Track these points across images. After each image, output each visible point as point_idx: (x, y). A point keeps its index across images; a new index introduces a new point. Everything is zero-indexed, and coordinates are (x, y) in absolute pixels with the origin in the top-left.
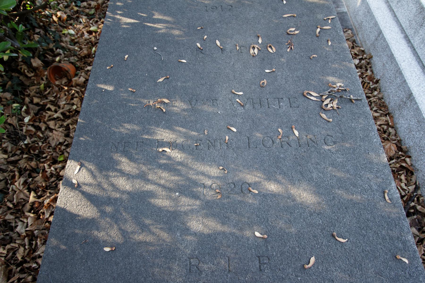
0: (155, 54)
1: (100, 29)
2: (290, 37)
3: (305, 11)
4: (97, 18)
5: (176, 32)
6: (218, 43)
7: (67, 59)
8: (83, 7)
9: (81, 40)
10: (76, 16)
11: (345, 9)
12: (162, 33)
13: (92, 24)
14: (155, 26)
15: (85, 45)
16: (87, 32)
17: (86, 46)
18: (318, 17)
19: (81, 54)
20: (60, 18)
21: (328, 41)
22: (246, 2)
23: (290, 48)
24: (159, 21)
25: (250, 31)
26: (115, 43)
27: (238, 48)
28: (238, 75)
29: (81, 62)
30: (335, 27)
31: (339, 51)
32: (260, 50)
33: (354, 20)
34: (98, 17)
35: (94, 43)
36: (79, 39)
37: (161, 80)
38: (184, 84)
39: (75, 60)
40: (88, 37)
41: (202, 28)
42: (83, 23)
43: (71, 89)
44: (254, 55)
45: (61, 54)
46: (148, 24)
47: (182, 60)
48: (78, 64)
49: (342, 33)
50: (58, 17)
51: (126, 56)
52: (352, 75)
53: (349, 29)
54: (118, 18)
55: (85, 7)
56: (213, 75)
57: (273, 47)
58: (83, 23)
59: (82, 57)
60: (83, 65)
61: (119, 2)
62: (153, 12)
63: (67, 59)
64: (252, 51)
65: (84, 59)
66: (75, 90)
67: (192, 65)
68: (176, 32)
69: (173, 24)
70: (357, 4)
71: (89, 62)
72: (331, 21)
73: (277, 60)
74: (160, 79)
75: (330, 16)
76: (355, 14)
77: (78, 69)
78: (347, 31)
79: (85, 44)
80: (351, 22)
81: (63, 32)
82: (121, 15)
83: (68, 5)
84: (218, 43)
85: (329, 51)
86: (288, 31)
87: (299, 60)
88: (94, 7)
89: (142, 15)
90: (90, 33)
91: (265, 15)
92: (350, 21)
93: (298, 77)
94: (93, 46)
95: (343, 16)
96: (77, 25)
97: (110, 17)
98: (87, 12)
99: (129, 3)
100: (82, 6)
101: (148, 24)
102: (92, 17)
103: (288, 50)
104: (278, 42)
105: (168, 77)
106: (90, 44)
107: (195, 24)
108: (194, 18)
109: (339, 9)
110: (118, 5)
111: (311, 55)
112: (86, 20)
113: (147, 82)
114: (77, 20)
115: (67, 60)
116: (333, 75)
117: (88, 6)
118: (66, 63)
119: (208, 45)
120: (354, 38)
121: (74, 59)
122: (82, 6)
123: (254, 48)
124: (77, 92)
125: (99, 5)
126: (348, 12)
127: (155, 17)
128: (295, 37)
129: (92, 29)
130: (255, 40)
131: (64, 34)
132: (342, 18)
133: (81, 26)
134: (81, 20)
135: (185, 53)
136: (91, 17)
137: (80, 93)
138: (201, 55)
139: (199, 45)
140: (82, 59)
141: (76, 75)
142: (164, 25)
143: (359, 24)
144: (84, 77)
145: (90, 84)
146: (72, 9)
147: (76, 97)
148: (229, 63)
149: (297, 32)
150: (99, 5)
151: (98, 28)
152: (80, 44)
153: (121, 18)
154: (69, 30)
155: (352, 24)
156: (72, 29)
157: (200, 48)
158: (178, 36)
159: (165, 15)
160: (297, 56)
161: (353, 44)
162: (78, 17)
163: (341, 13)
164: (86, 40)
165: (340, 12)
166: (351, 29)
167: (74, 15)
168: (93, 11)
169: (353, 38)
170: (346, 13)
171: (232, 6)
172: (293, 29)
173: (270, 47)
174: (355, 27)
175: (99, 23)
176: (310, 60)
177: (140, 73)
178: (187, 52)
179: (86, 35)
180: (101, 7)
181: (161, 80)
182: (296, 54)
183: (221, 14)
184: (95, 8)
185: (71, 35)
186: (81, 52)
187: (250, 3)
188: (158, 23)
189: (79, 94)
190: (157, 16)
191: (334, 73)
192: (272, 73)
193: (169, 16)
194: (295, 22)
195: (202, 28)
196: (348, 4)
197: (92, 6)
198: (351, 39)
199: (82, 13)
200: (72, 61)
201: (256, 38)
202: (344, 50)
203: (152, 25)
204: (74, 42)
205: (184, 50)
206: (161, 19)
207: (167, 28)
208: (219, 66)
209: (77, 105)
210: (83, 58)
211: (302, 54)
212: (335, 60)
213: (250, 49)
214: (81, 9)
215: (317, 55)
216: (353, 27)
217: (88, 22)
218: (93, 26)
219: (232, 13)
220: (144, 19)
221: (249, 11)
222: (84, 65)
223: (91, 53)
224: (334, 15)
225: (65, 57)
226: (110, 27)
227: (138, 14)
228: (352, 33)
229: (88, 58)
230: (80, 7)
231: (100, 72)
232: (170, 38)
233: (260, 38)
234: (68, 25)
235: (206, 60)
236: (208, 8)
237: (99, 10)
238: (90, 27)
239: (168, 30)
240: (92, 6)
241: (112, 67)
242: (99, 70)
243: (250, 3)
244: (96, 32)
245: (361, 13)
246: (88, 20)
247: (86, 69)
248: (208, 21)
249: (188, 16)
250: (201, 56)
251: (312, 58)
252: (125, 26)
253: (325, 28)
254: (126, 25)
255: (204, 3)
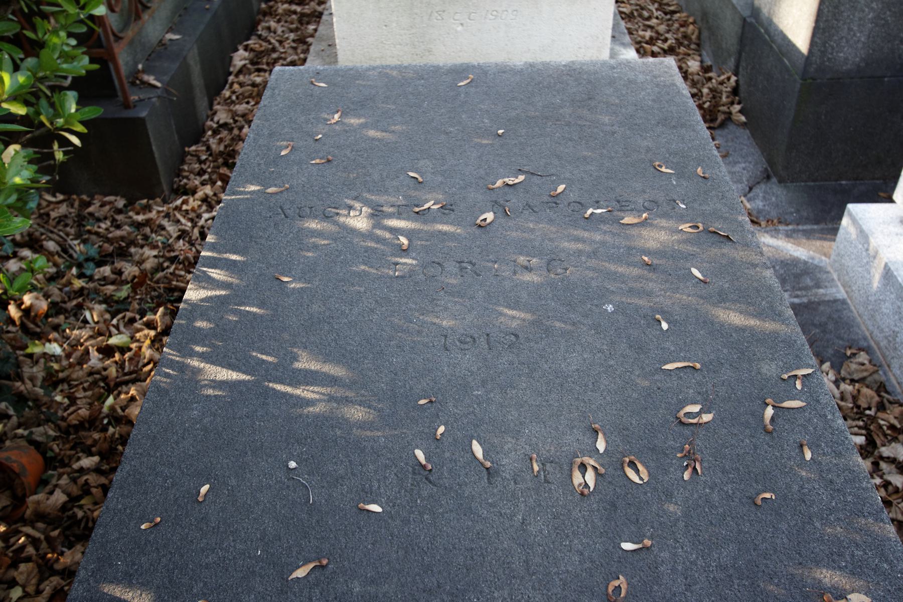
0: (291, 483)
1: (138, 341)
2: (687, 432)
3: (725, 351)
4: (132, 311)
5: (357, 413)
6: (478, 450)
7: (26, 433)
8: (99, 280)
9: (78, 373)
10: (74, 302)
11: (838, 292)
12: (317, 416)
13: (117, 327)
14: (298, 392)
15: (85, 390)
16: (99, 350)
17: (89, 393)
18: (764, 371)
19: (71, 418)
20: (27, 312)
21: (801, 446)
22: (558, 324)
23: (690, 469)
24: (309, 378)
25: (570, 412)
26: (177, 443)
27: (536, 468)
28: (537, 560)
29: (66, 441)
30: (818, 401)
31: (839, 481)
32: (601, 475)
33: (869, 323)
34: (137, 306)
35: (112, 384)
36: (71, 370)
37: (301, 573)
38: (371, 589)
39: (48, 436)
40: (100, 365)
41: (431, 402)
42: (93, 325)
43: (17, 533)
44: (586, 491)
45: (9, 417)
46: (279, 387)
47: (369, 503)
48: (55, 447)
49: (841, 421)
50: (23, 307)
51: (204, 489)
52: (890, 563)
53: (861, 349)
54: (194, 367)
55: (104, 278)
56: (461, 559)
57: (640, 467)
58: (93, 325)
59: (69, 426)
60: (68, 453)
61: (203, 320)
62: (295, 350)
63: (26, 433)
64: (577, 478)
65: (76, 432)
66: (28, 536)
67: (398, 522)
68: (357, 413)
69: (350, 388)
70: (870, 283)
71: (89, 442)
72: (803, 385)
73: (654, 508)
74: (298, 567)
75: (798, 368)
76: (870, 307)
77: (51, 462)
78: (854, 355)
79: (86, 385)
80: (864, 328)
81: (29, 351)
82: (203, 357)
83: (57, 273)
84: (478, 450)
85: (809, 480)
86: (682, 413)
87: (721, 510)
88: (129, 279)
89: (264, 357)
90: (107, 351)
91: (612, 362)
92: (859, 327)
93: (722, 568)
94: (109, 391)
95: (837, 311)
96: (72, 329)
97: (171, 364)
98: (108, 292)
99: (230, 321)
100: (96, 277)
101: (279, 387)
102: (121, 307)
103: (686, 476)
104: (653, 449)
105: (325, 562)
106: (102, 384)
107: (411, 388)
108: (411, 369)
109: (821, 291)
110: (200, 329)
111: (758, 494)
112: (101, 315)
113: (258, 579)
114: (75, 315)
115: (22, 436)
116: (832, 562)
117: (113, 276)
118: (19, 448)
119: (447, 455)
120: (880, 377)
121: (46, 433)
122: (96, 277)
123: (583, 468)
124: (34, 542)
125: (144, 273)
126: (849, 301)
127: (298, 365)
128: (702, 432)
129: (114, 341)
130: (587, 440)
131: (30, 356)
132: (835, 316)
133: (85, 333)
134: (87, 314)
135: (379, 481)
136: (116, 307)
137: (44, 545)
138: (427, 490)
139: (420, 455)
140: (67, 433)
141: (43, 483)
142: (323, 390)
143: (886, 337)
144: (64, 492)
145: (80, 582)
146: (70, 283)
147: (28, 559)
148: (511, 517)
149: (707, 418)
150: (144, 273)
151: (132, 338)
152: (71, 386)
153: (202, 365)
154: (47, 345)
155: (867, 334)
156: (56, 340)
157: (424, 467)
158: (362, 425)
159: (327, 358)
160: (715, 497)
161: (879, 396)
162: (80, 307)
163: (829, 301)
164: (91, 374)
165: (827, 299)
166: (868, 350)
167: (70, 300)
168: (124, 292)
169: (876, 376)
170: (844, 302)
171: (516, 336)
172: (696, 408)
173: (632, 464)
174: (878, 344)
175: (137, 325)
176: (753, 508)
177: (239, 546)
178: (385, 478)
179: (94, 355)
180: (151, 280)
181: (301, 573)
182: (711, 488)
183: (485, 360)
184: (132, 281)
185: (49, 357)
186: (72, 409)
187: (569, 327)
188: (307, 385)
189: (37, 549)
190: (305, 363)
191: (835, 557)
192: (643, 554)
193: (337, 362)
194: (699, 384)
195: (431, 402)
196: (847, 278)
197: (123, 278)
198: (869, 379)
199: (92, 296)
200: (39, 439)
201: (588, 434)
202: (853, 477)
203: (289, 389)
204: (52, 381)
205: (376, 472)
206: (316, 372)
207: (331, 398)
208: (479, 527)
209: (24, 587)
210: (72, 430)
211: (729, 488)
212: (831, 511)
213: (571, 470)
214: (91, 285)
215: (773, 491)
216: (873, 344)
217: (105, 321)
218: (120, 333)
219: (517, 355)
220: (267, 370)
221: (567, 351)
222: (73, 452)
223: (101, 412)
224: (809, 366)
225: (19, 426)
226: (167, 392)
227: (251, 356)
228: (870, 362)
229: (89, 430)
230: (91, 278)
231: (118, 539)
232: (339, 433)
233: (600, 435)
234: (48, 329)
235: (441, 505)
236: (449, 340)
237: (143, 289)
238: (110, 336)
239: (335, 405)
240: (123, 278)
241: (157, 525)
242: (116, 535)
243: (569, 327)
244: (123, 350)
245: (886, 308)
246: (108, 316)
247: (76, 466)
248: (449, 381)
249: (391, 363)
250: (425, 493)
251: (759, 502)
252: (210, 392)
253: (787, 404)
254: (214, 388)
255: (440, 326)
